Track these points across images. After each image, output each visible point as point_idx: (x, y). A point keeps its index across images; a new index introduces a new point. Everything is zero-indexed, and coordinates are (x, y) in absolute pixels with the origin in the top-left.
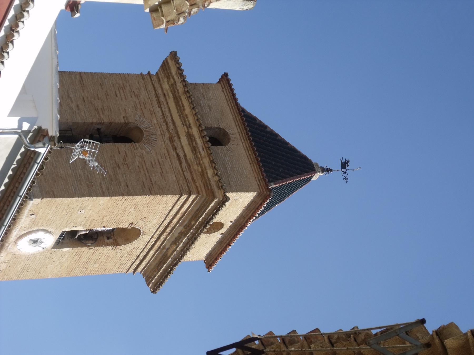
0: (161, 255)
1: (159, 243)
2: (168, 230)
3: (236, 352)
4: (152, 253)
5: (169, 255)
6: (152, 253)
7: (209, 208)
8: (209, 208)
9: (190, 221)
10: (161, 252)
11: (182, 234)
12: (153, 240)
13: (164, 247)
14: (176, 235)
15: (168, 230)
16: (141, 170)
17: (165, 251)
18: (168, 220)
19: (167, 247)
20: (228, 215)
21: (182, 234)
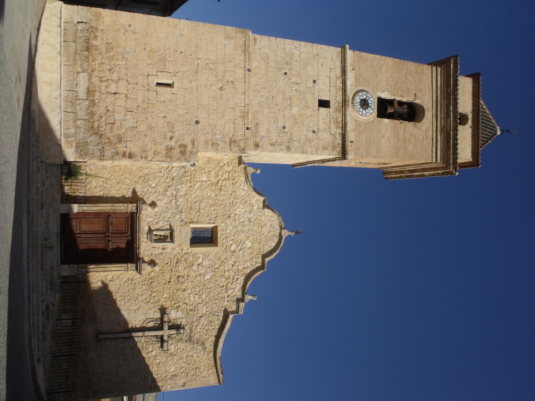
0: (445, 135)
1: (439, 125)
2: (439, 109)
3: (475, 77)
4: (439, 137)
5: (449, 130)
6: (439, 143)
7: (452, 70)
8: (452, 70)
9: (447, 91)
10: (443, 133)
11: (448, 106)
12: (434, 120)
13: (444, 127)
14: (445, 110)
15: (439, 109)
16: (41, 328)
17: (445, 129)
18: (434, 95)
19: (445, 125)
20: (465, 135)
21: (448, 106)
